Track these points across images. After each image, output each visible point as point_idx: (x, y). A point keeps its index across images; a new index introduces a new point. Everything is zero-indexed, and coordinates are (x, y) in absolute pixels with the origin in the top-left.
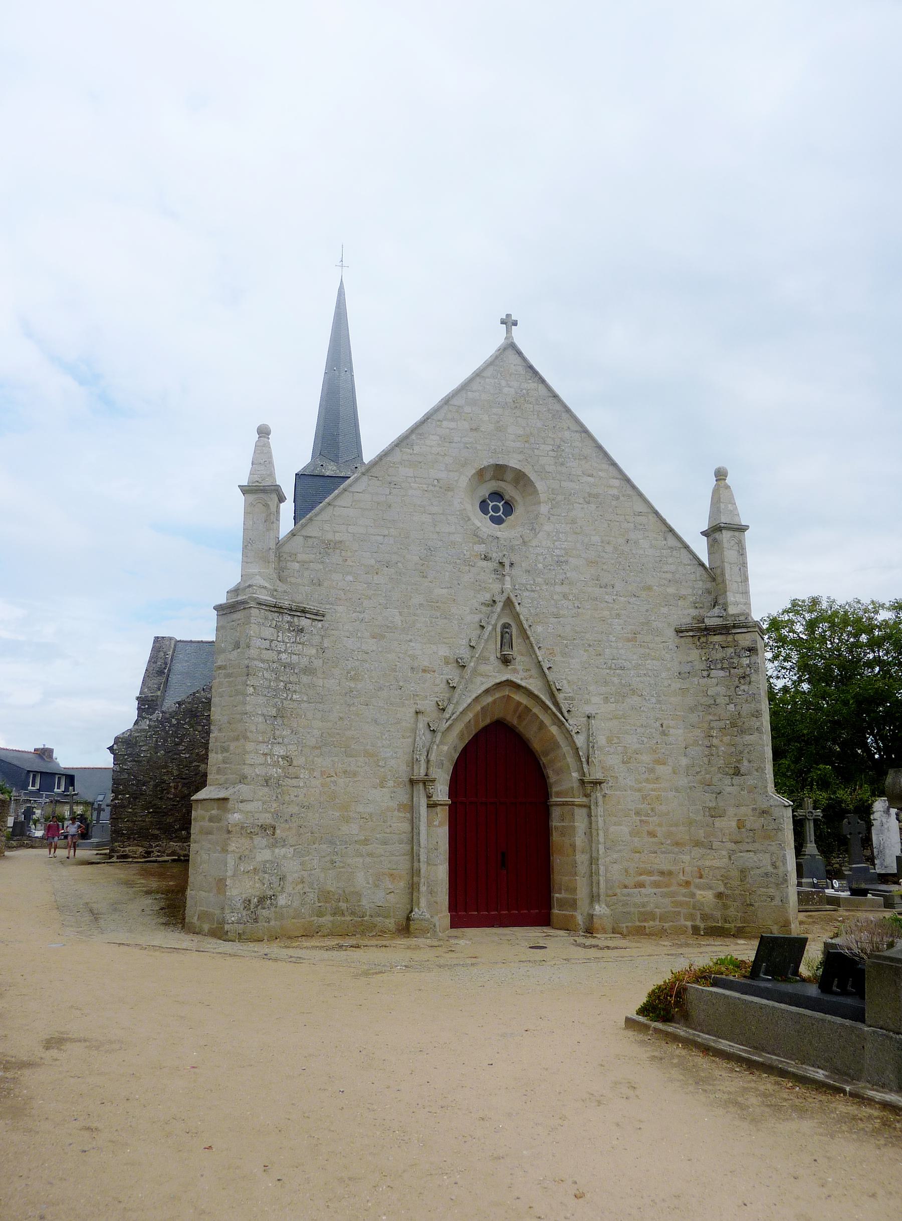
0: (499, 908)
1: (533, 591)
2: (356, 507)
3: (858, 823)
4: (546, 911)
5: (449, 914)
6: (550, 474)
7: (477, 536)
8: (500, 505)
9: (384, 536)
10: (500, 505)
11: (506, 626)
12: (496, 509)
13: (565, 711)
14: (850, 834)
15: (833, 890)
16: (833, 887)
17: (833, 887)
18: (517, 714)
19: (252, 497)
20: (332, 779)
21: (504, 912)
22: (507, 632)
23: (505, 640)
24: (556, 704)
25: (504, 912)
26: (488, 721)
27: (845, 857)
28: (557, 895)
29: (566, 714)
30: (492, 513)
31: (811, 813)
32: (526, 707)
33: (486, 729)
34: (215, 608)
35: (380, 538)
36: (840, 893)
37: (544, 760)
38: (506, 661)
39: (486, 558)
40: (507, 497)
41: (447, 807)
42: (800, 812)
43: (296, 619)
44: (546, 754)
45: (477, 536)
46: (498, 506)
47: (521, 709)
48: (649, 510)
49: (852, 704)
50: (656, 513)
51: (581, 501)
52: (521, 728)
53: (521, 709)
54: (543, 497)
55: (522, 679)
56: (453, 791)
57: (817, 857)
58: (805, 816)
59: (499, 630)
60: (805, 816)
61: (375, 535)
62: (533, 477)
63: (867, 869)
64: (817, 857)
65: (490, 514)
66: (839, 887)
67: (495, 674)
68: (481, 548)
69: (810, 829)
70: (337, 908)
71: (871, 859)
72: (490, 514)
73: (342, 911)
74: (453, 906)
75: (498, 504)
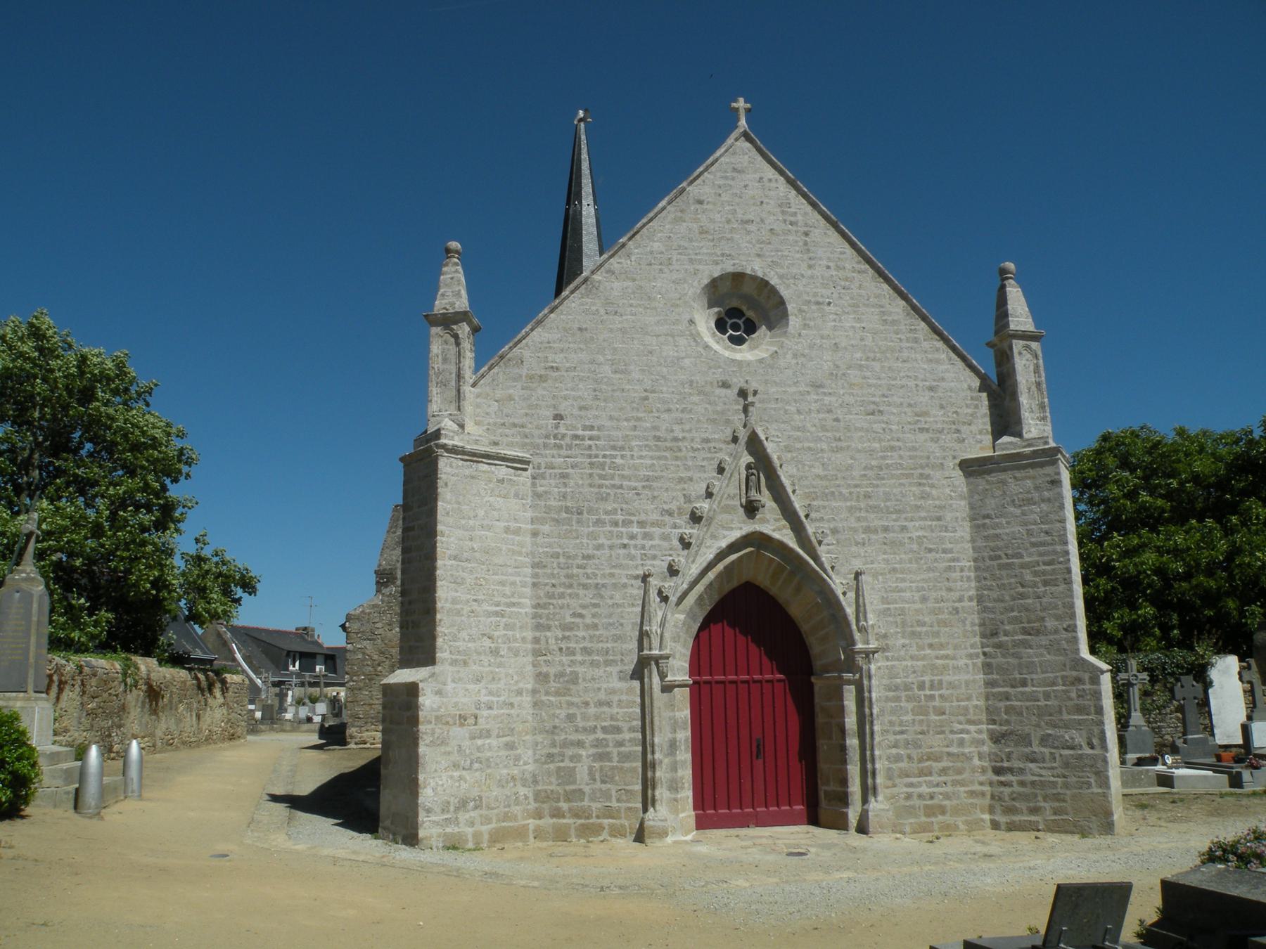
3: (1193, 686)
5: (693, 813)
8: (740, 322)
10: (740, 322)
13: (828, 567)
14: (1184, 699)
15: (1165, 767)
16: (1164, 764)
17: (1164, 764)
19: (1125, 798)
23: (751, 484)
26: (735, 584)
27: (1178, 727)
28: (824, 788)
29: (829, 570)
31: (1136, 676)
33: (733, 593)
34: (402, 459)
36: (1173, 770)
38: (751, 509)
39: (725, 385)
41: (688, 689)
42: (1123, 676)
46: (738, 120)
49: (1140, 537)
55: (774, 530)
56: (696, 666)
57: (1143, 728)
58: (1128, 680)
60: (1128, 680)
63: (1204, 741)
64: (1143, 728)
66: (1173, 763)
67: (739, 528)
68: (719, 375)
69: (1135, 693)
70: (558, 809)
71: (1210, 729)
72: (728, 334)
73: (564, 812)
74: (701, 802)
75: (733, 333)
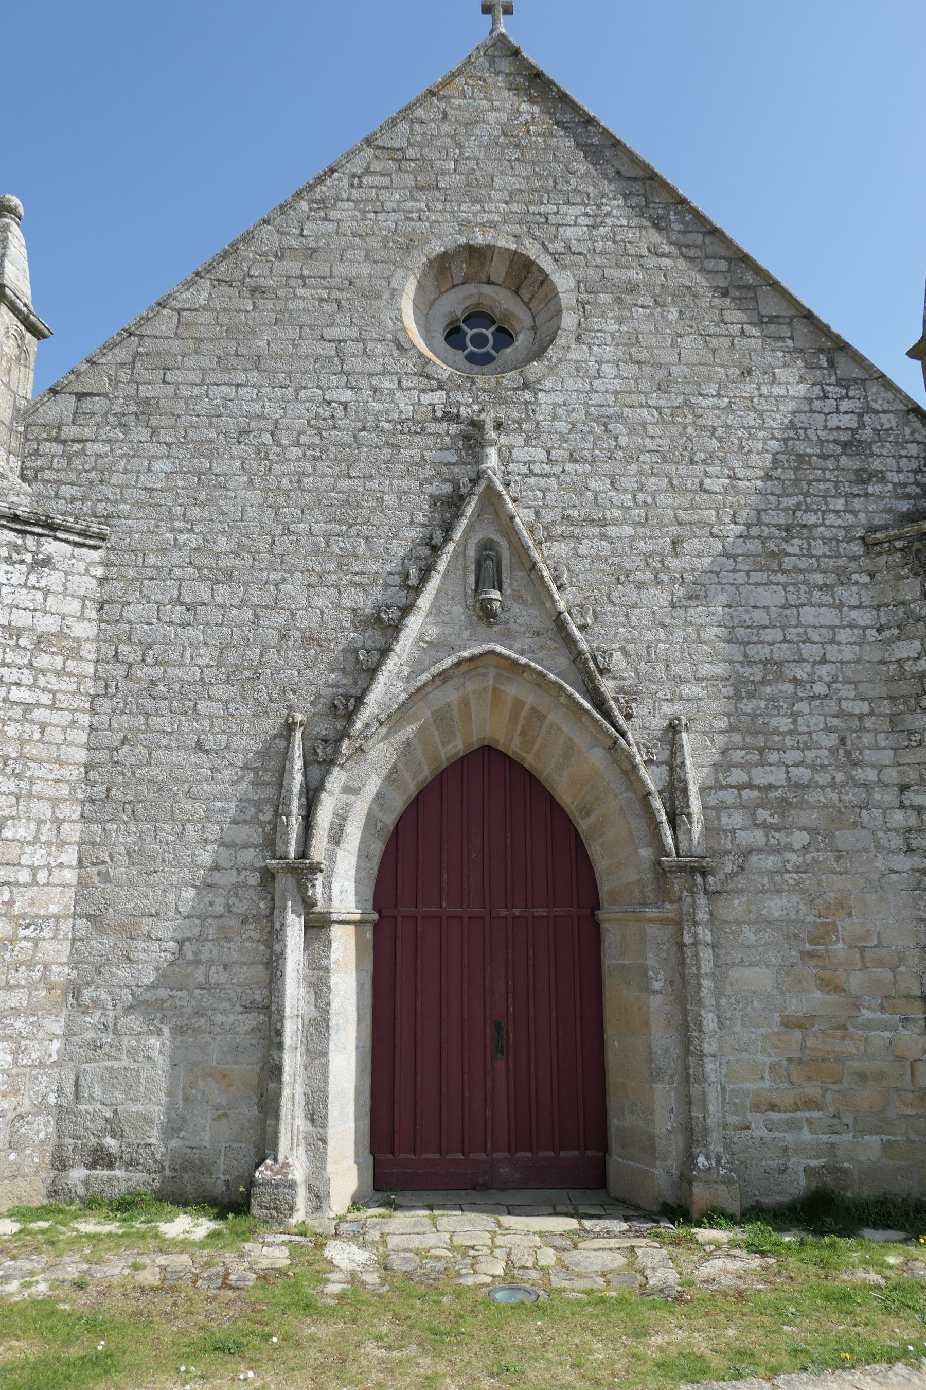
0: (489, 1146)
1: (547, 476)
2: (184, 335)
4: (595, 1154)
6: (581, 257)
7: (428, 377)
9: (238, 385)
10: (488, 333)
11: (487, 546)
12: (479, 341)
18: (519, 729)
20: (102, 868)
21: (430, 1156)
22: (488, 556)
23: (484, 574)
24: (600, 703)
25: (430, 1156)
29: (621, 720)
30: (471, 348)
32: (533, 709)
35: (231, 391)
37: (583, 825)
40: (497, 315)
43: (30, 541)
44: (586, 811)
45: (428, 377)
47: (524, 713)
48: (792, 312)
50: (809, 316)
51: (649, 301)
52: (529, 760)
53: (524, 713)
54: (567, 299)
59: (472, 553)
61: (218, 385)
62: (546, 263)
65: (467, 351)
72: (467, 351)
75: (484, 331)
